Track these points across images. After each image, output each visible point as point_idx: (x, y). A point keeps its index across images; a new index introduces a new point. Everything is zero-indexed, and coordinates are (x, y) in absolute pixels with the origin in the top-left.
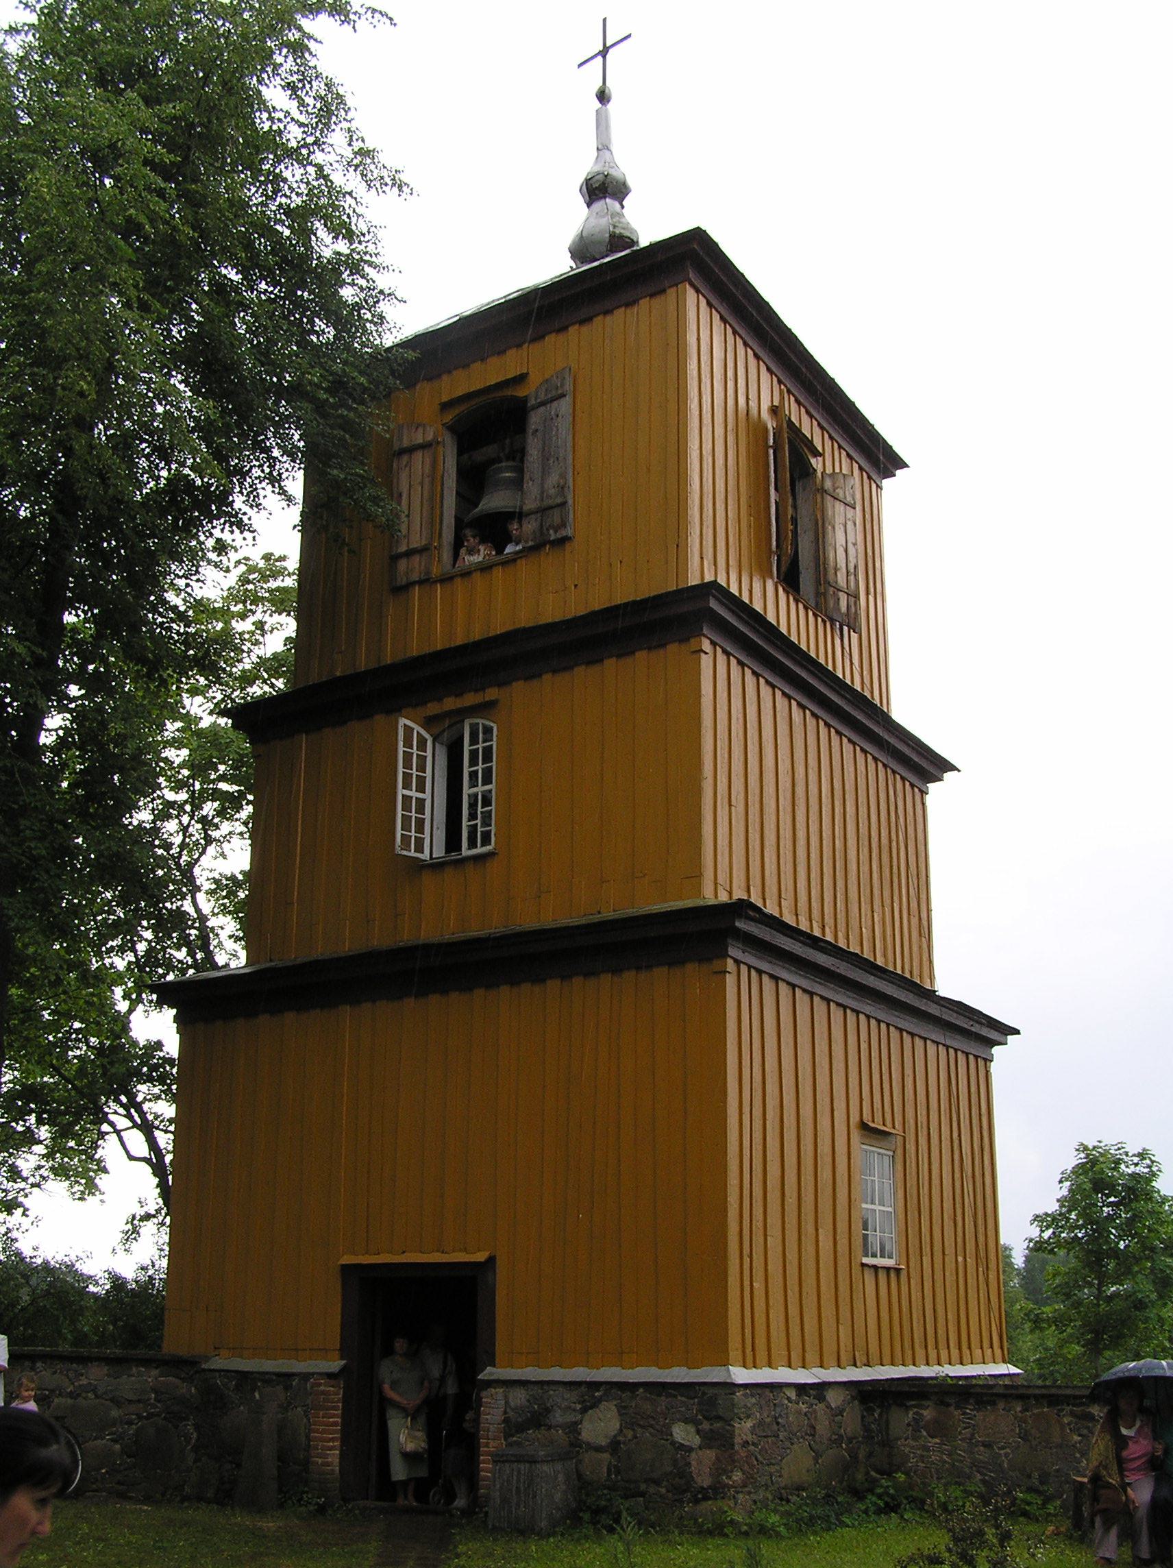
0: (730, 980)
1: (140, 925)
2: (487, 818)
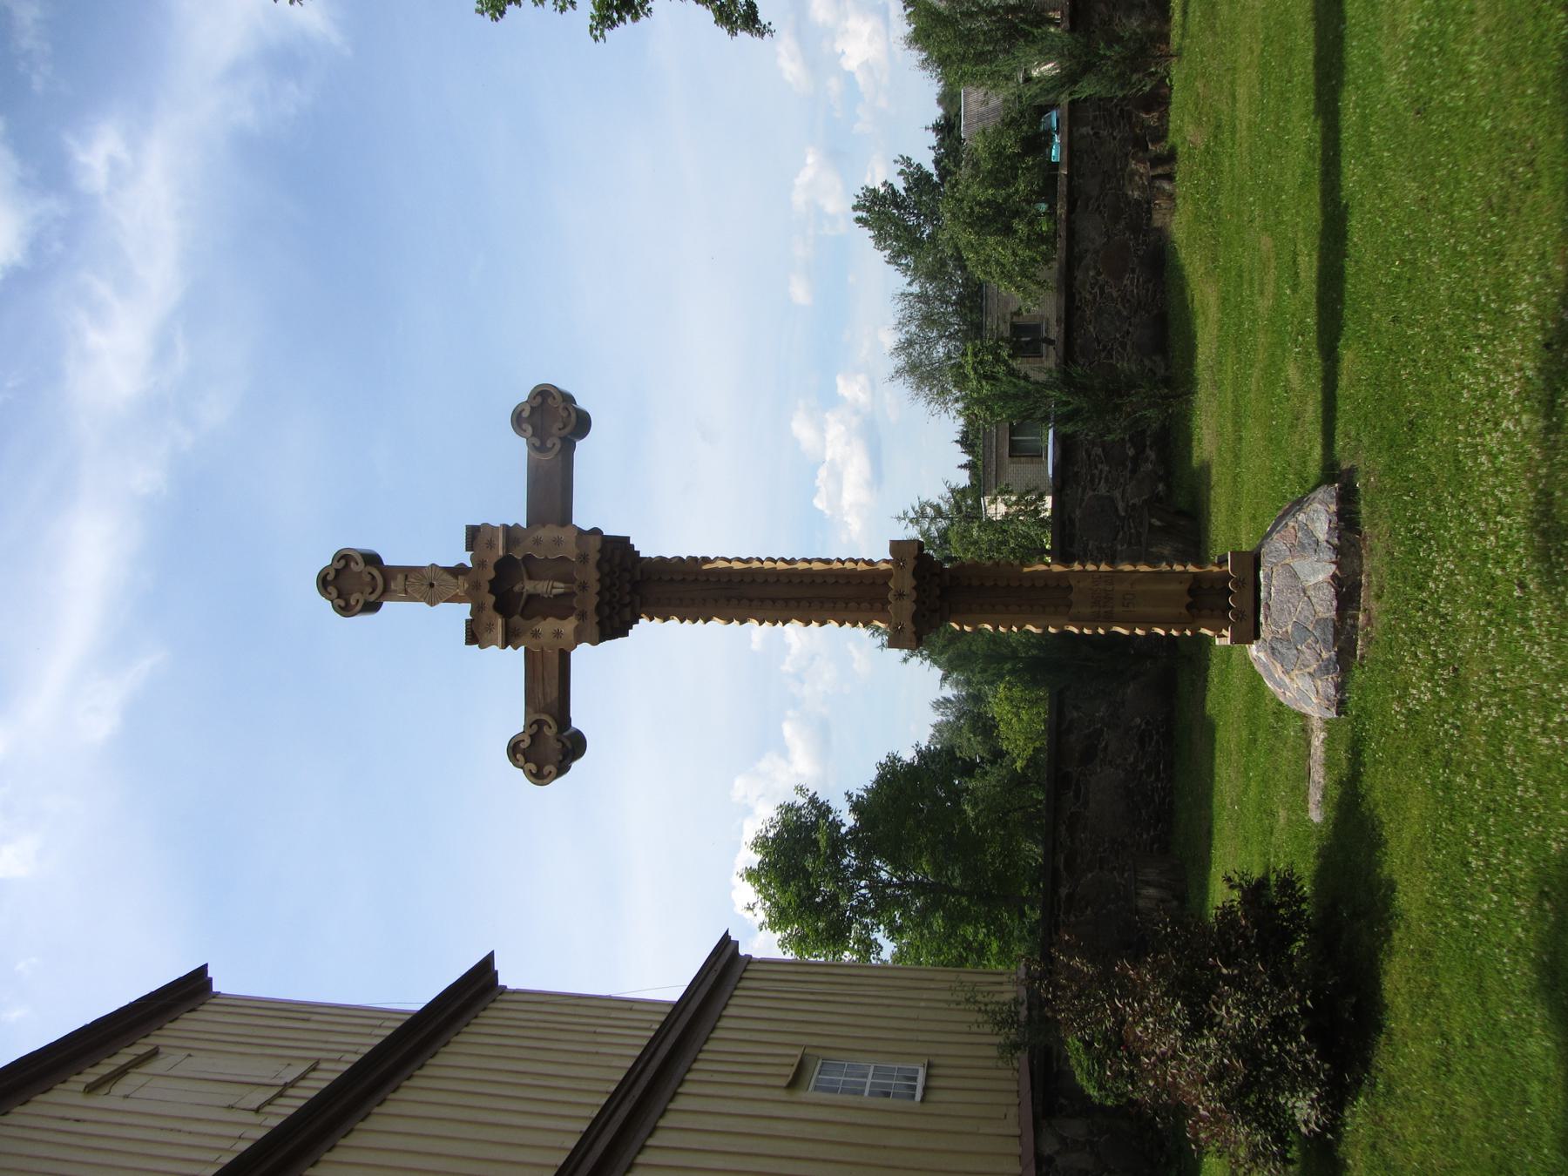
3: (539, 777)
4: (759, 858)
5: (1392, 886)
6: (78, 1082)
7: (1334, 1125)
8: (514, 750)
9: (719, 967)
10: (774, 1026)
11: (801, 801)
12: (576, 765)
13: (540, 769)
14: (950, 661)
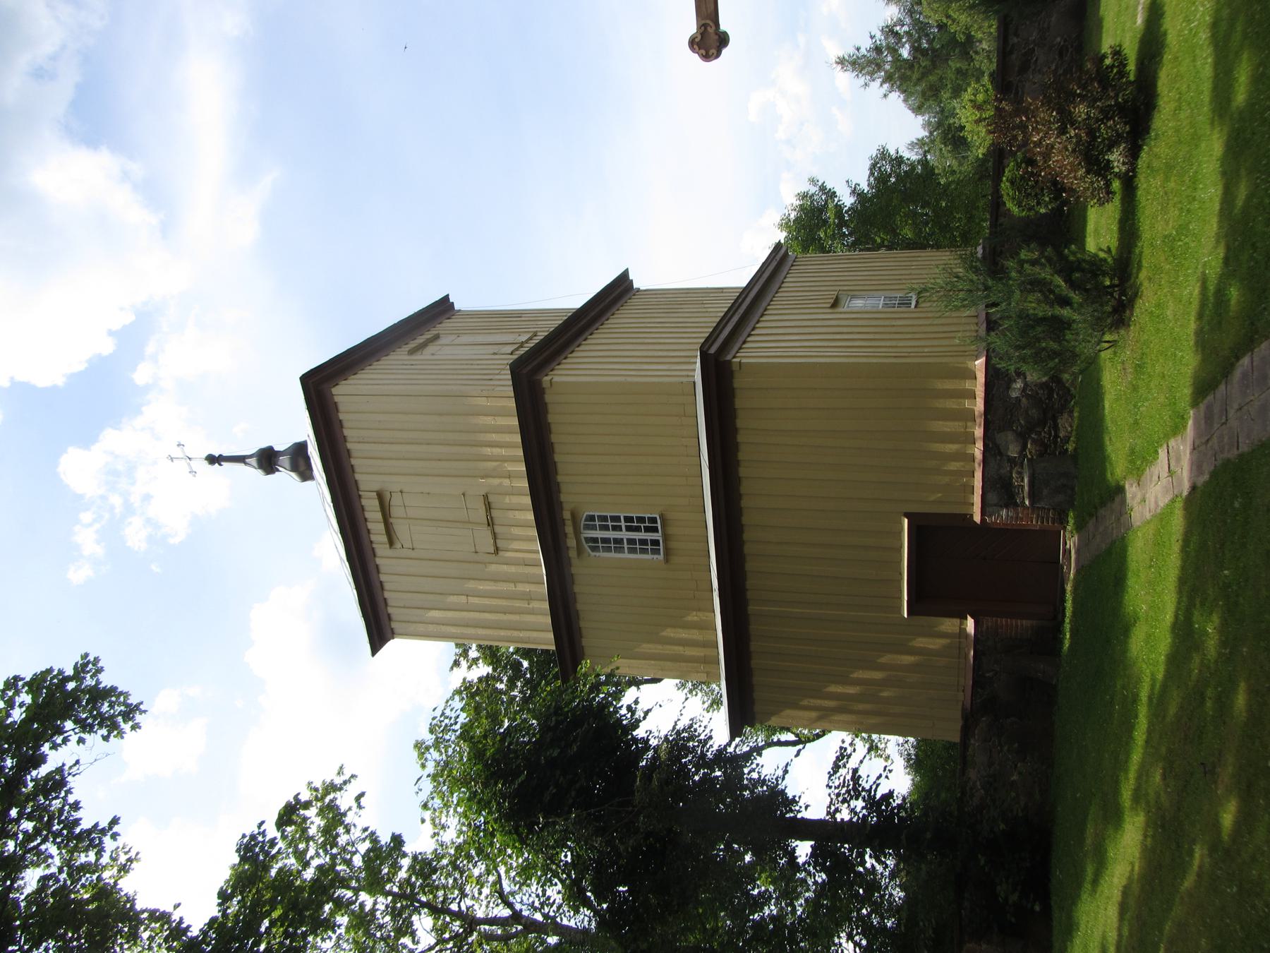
0: (744, 360)
1: (886, 811)
2: (641, 520)
3: (707, 57)
4: (784, 234)
5: (1165, 34)
6: (406, 348)
7: (1133, 168)
8: (692, 43)
9: (778, 258)
10: (812, 330)
11: (813, 190)
12: (724, 51)
13: (707, 53)
14: (923, 93)
